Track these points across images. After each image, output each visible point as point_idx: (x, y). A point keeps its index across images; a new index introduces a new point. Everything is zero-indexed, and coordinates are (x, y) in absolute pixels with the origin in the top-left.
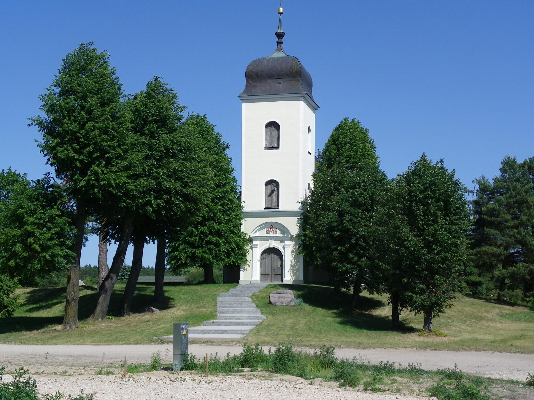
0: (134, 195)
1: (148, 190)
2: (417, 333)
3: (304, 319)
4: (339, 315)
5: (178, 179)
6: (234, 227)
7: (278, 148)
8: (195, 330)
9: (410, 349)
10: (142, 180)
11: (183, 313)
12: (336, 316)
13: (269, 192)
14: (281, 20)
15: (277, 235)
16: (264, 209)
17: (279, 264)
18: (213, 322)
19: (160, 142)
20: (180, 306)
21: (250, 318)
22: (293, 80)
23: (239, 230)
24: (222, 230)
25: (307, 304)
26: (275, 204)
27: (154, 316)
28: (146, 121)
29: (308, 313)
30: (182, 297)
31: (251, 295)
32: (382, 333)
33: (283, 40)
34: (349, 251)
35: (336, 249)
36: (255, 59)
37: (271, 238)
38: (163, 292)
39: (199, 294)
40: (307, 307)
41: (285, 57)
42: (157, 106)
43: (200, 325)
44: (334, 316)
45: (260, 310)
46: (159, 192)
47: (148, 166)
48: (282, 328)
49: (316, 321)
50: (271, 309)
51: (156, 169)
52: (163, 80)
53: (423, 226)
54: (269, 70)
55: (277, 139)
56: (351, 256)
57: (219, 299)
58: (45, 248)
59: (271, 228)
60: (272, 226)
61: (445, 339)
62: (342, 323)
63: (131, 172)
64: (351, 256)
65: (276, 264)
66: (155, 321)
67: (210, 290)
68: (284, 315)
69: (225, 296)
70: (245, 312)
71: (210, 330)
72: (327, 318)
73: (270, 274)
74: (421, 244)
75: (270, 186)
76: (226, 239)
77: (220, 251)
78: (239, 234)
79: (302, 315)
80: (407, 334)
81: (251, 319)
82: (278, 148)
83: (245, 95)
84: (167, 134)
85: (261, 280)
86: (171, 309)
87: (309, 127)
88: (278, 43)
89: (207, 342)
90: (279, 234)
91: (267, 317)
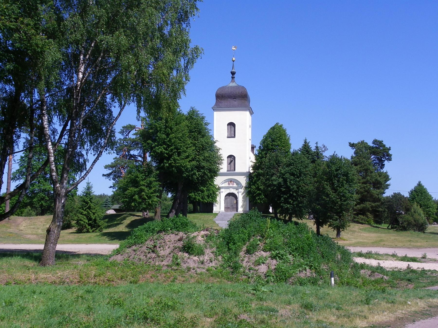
7: (234, 137)
13: (229, 162)
14: (234, 64)
15: (234, 186)
26: (233, 168)
33: (235, 76)
34: (289, 198)
35: (283, 197)
37: (231, 187)
46: (199, 168)
52: (197, 108)
58: (149, 198)
59: (231, 182)
60: (231, 181)
61: (348, 242)
73: (230, 207)
75: (230, 158)
76: (207, 188)
77: (204, 195)
78: (214, 186)
82: (234, 137)
90: (235, 185)
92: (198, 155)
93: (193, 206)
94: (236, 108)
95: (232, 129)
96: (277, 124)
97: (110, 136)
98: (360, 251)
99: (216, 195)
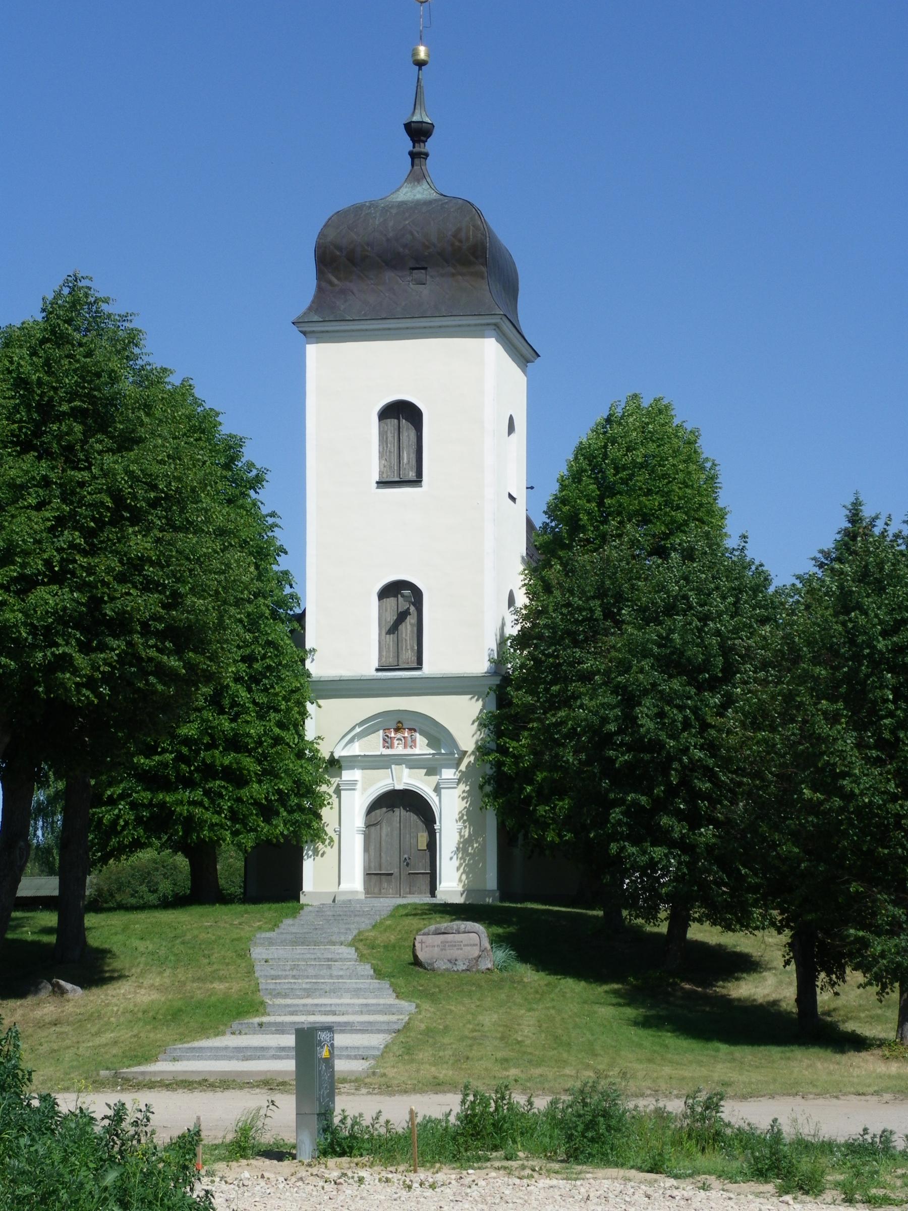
0: (17, 641)
1: (60, 620)
2: (878, 1052)
3: (530, 1010)
4: (630, 998)
5: (148, 586)
6: (281, 725)
7: (417, 481)
8: (217, 1048)
9: (875, 1098)
10: (41, 592)
11: (155, 996)
12: (621, 1001)
13: (391, 618)
14: (423, 83)
15: (417, 751)
16: (377, 670)
17: (423, 839)
18: (261, 1025)
19: (94, 477)
20: (142, 974)
21: (366, 1009)
22: (462, 274)
23: (297, 733)
24: (248, 735)
25: (529, 966)
26: (408, 655)
27: (69, 1008)
28: (47, 411)
29: (537, 992)
30: (141, 946)
31: (350, 938)
32: (775, 1052)
33: (430, 146)
36: (344, 204)
37: (400, 760)
38: (81, 930)
39: (188, 937)
40: (529, 975)
41: (435, 200)
42: (84, 367)
43: (223, 1033)
44: (614, 1001)
45: (392, 985)
47: (60, 550)
48: (474, 1038)
49: (566, 1016)
50: (422, 982)
51: (85, 557)
52: (100, 288)
53: (893, 732)
54: (388, 240)
55: (413, 456)
56: (665, 821)
57: (258, 952)
59: (397, 730)
62: (645, 1023)
63: (15, 571)
64: (665, 821)
65: (413, 841)
66: (81, 1022)
67: (222, 925)
68: (466, 1001)
69: (271, 942)
70: (348, 991)
71: (263, 1049)
72: (596, 1008)
73: (395, 871)
74: (892, 787)
79: (519, 999)
80: (851, 1053)
81: (369, 1013)
82: (417, 481)
83: (316, 318)
84: (113, 452)
85: (367, 890)
86: (116, 985)
87: (511, 419)
88: (413, 155)
89: (200, 1083)
90: (421, 747)
91: (417, 1006)
92: (85, 553)
93: (192, 864)
94: (437, 322)
95: (404, 437)
97: (675, 694)
98: (876, 1129)
99: (319, 801)
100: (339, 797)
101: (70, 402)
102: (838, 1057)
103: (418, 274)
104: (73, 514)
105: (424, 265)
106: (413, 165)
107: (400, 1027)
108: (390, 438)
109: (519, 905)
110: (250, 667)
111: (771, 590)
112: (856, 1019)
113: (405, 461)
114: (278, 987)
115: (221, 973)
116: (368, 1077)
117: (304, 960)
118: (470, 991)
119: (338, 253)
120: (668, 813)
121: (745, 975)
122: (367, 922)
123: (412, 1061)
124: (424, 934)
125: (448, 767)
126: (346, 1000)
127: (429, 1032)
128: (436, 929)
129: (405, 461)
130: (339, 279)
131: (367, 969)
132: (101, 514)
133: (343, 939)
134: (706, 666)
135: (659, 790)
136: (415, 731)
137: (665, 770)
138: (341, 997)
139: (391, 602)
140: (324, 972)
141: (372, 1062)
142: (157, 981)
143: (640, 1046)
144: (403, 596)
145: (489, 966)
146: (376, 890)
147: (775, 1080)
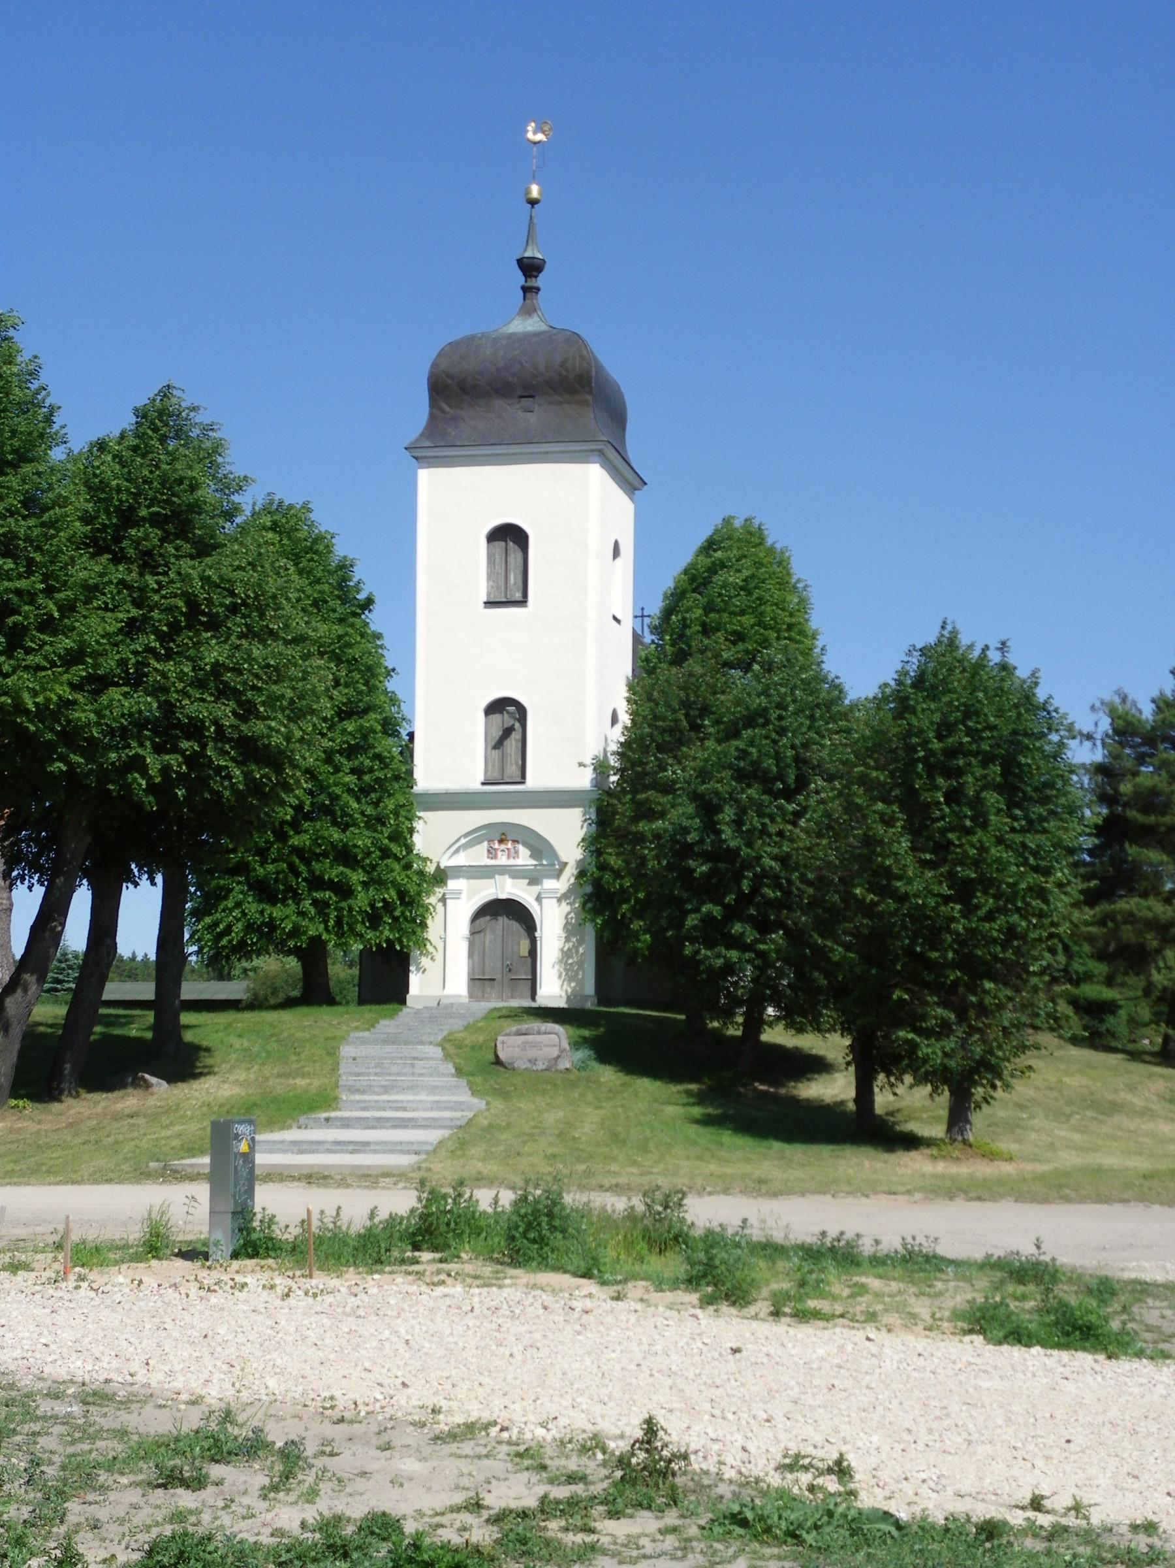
0: (91, 740)
2: (927, 1151)
3: (597, 1108)
7: (523, 602)
8: (274, 1142)
9: (906, 1197)
10: (115, 693)
11: (237, 1090)
12: (692, 1100)
13: (497, 734)
14: (535, 221)
15: (519, 862)
16: (483, 784)
17: (524, 948)
18: (327, 1120)
20: (230, 1070)
21: (437, 1105)
22: (569, 403)
24: (355, 846)
26: (513, 770)
27: (152, 1101)
29: (610, 1091)
30: (237, 1043)
31: (439, 1038)
32: (825, 1150)
33: (541, 281)
38: (178, 1028)
39: (285, 1035)
40: (608, 1075)
41: (545, 332)
43: (289, 1127)
45: (469, 1083)
47: (135, 653)
48: (532, 1135)
52: (185, 397)
57: (346, 1051)
59: (501, 841)
60: (503, 835)
61: (1007, 1168)
62: (706, 1121)
64: (737, 928)
66: (155, 1117)
68: (539, 1099)
69: (363, 1042)
71: (318, 1143)
72: (664, 1107)
73: (498, 976)
82: (523, 602)
84: (192, 557)
86: (202, 1079)
87: (616, 544)
88: (526, 290)
90: (524, 858)
91: (488, 1104)
92: (158, 657)
93: (304, 967)
94: (544, 448)
95: (511, 559)
96: (727, 521)
100: (445, 905)
101: (148, 507)
102: (886, 1156)
103: (526, 402)
104: (146, 619)
105: (531, 392)
106: (525, 298)
107: (463, 1123)
108: (498, 560)
109: (612, 1010)
110: (359, 779)
111: (847, 702)
112: (920, 1119)
113: (512, 581)
114: (358, 1083)
115: (306, 1069)
116: (413, 1171)
117: (391, 1058)
118: (545, 1090)
119: (449, 381)
120: (741, 920)
121: (816, 1076)
122: (460, 1023)
123: (463, 1156)
124: (506, 1035)
125: (550, 877)
126: (423, 1097)
127: (490, 1128)
128: (518, 1030)
129: (512, 581)
130: (450, 407)
131: (450, 1068)
132: (175, 618)
133: (432, 1039)
134: (781, 777)
135: (730, 898)
136: (518, 842)
137: (738, 877)
138: (418, 1094)
139: (496, 718)
140: (407, 1070)
141: (423, 1157)
142: (243, 1076)
143: (695, 1143)
144: (508, 712)
145: (568, 1065)
146: (480, 995)
147: (813, 1178)
